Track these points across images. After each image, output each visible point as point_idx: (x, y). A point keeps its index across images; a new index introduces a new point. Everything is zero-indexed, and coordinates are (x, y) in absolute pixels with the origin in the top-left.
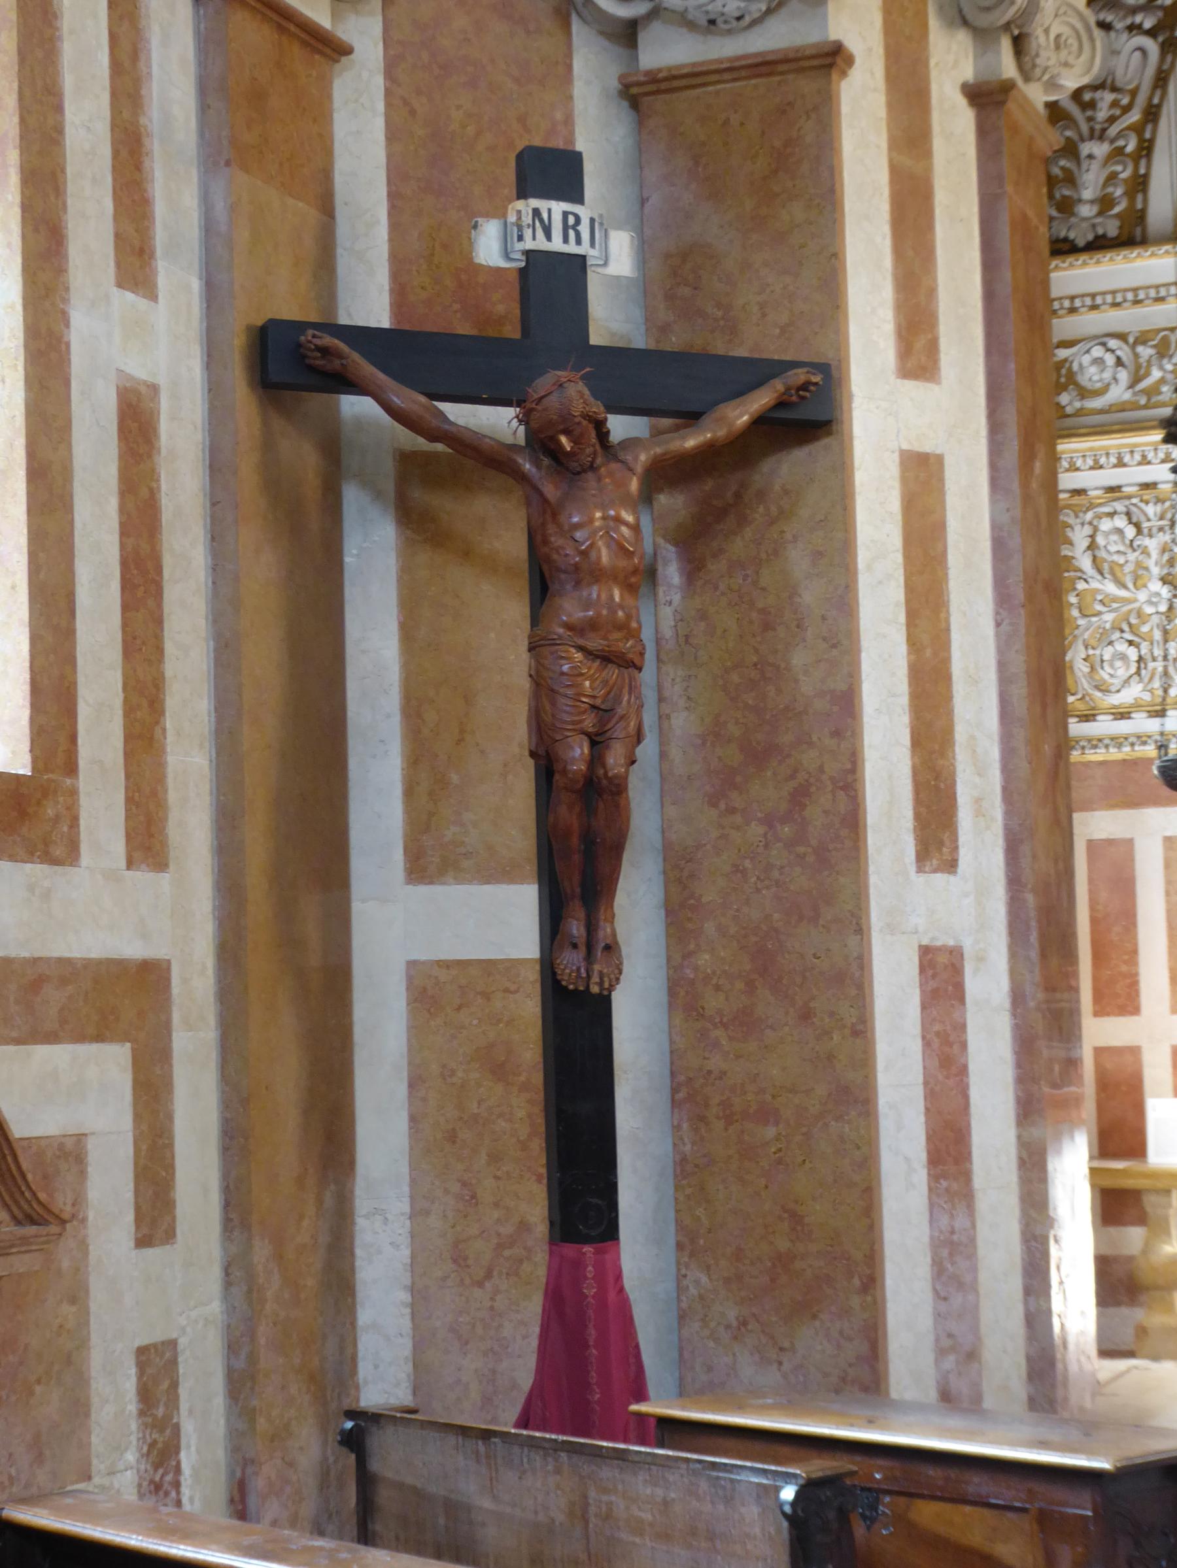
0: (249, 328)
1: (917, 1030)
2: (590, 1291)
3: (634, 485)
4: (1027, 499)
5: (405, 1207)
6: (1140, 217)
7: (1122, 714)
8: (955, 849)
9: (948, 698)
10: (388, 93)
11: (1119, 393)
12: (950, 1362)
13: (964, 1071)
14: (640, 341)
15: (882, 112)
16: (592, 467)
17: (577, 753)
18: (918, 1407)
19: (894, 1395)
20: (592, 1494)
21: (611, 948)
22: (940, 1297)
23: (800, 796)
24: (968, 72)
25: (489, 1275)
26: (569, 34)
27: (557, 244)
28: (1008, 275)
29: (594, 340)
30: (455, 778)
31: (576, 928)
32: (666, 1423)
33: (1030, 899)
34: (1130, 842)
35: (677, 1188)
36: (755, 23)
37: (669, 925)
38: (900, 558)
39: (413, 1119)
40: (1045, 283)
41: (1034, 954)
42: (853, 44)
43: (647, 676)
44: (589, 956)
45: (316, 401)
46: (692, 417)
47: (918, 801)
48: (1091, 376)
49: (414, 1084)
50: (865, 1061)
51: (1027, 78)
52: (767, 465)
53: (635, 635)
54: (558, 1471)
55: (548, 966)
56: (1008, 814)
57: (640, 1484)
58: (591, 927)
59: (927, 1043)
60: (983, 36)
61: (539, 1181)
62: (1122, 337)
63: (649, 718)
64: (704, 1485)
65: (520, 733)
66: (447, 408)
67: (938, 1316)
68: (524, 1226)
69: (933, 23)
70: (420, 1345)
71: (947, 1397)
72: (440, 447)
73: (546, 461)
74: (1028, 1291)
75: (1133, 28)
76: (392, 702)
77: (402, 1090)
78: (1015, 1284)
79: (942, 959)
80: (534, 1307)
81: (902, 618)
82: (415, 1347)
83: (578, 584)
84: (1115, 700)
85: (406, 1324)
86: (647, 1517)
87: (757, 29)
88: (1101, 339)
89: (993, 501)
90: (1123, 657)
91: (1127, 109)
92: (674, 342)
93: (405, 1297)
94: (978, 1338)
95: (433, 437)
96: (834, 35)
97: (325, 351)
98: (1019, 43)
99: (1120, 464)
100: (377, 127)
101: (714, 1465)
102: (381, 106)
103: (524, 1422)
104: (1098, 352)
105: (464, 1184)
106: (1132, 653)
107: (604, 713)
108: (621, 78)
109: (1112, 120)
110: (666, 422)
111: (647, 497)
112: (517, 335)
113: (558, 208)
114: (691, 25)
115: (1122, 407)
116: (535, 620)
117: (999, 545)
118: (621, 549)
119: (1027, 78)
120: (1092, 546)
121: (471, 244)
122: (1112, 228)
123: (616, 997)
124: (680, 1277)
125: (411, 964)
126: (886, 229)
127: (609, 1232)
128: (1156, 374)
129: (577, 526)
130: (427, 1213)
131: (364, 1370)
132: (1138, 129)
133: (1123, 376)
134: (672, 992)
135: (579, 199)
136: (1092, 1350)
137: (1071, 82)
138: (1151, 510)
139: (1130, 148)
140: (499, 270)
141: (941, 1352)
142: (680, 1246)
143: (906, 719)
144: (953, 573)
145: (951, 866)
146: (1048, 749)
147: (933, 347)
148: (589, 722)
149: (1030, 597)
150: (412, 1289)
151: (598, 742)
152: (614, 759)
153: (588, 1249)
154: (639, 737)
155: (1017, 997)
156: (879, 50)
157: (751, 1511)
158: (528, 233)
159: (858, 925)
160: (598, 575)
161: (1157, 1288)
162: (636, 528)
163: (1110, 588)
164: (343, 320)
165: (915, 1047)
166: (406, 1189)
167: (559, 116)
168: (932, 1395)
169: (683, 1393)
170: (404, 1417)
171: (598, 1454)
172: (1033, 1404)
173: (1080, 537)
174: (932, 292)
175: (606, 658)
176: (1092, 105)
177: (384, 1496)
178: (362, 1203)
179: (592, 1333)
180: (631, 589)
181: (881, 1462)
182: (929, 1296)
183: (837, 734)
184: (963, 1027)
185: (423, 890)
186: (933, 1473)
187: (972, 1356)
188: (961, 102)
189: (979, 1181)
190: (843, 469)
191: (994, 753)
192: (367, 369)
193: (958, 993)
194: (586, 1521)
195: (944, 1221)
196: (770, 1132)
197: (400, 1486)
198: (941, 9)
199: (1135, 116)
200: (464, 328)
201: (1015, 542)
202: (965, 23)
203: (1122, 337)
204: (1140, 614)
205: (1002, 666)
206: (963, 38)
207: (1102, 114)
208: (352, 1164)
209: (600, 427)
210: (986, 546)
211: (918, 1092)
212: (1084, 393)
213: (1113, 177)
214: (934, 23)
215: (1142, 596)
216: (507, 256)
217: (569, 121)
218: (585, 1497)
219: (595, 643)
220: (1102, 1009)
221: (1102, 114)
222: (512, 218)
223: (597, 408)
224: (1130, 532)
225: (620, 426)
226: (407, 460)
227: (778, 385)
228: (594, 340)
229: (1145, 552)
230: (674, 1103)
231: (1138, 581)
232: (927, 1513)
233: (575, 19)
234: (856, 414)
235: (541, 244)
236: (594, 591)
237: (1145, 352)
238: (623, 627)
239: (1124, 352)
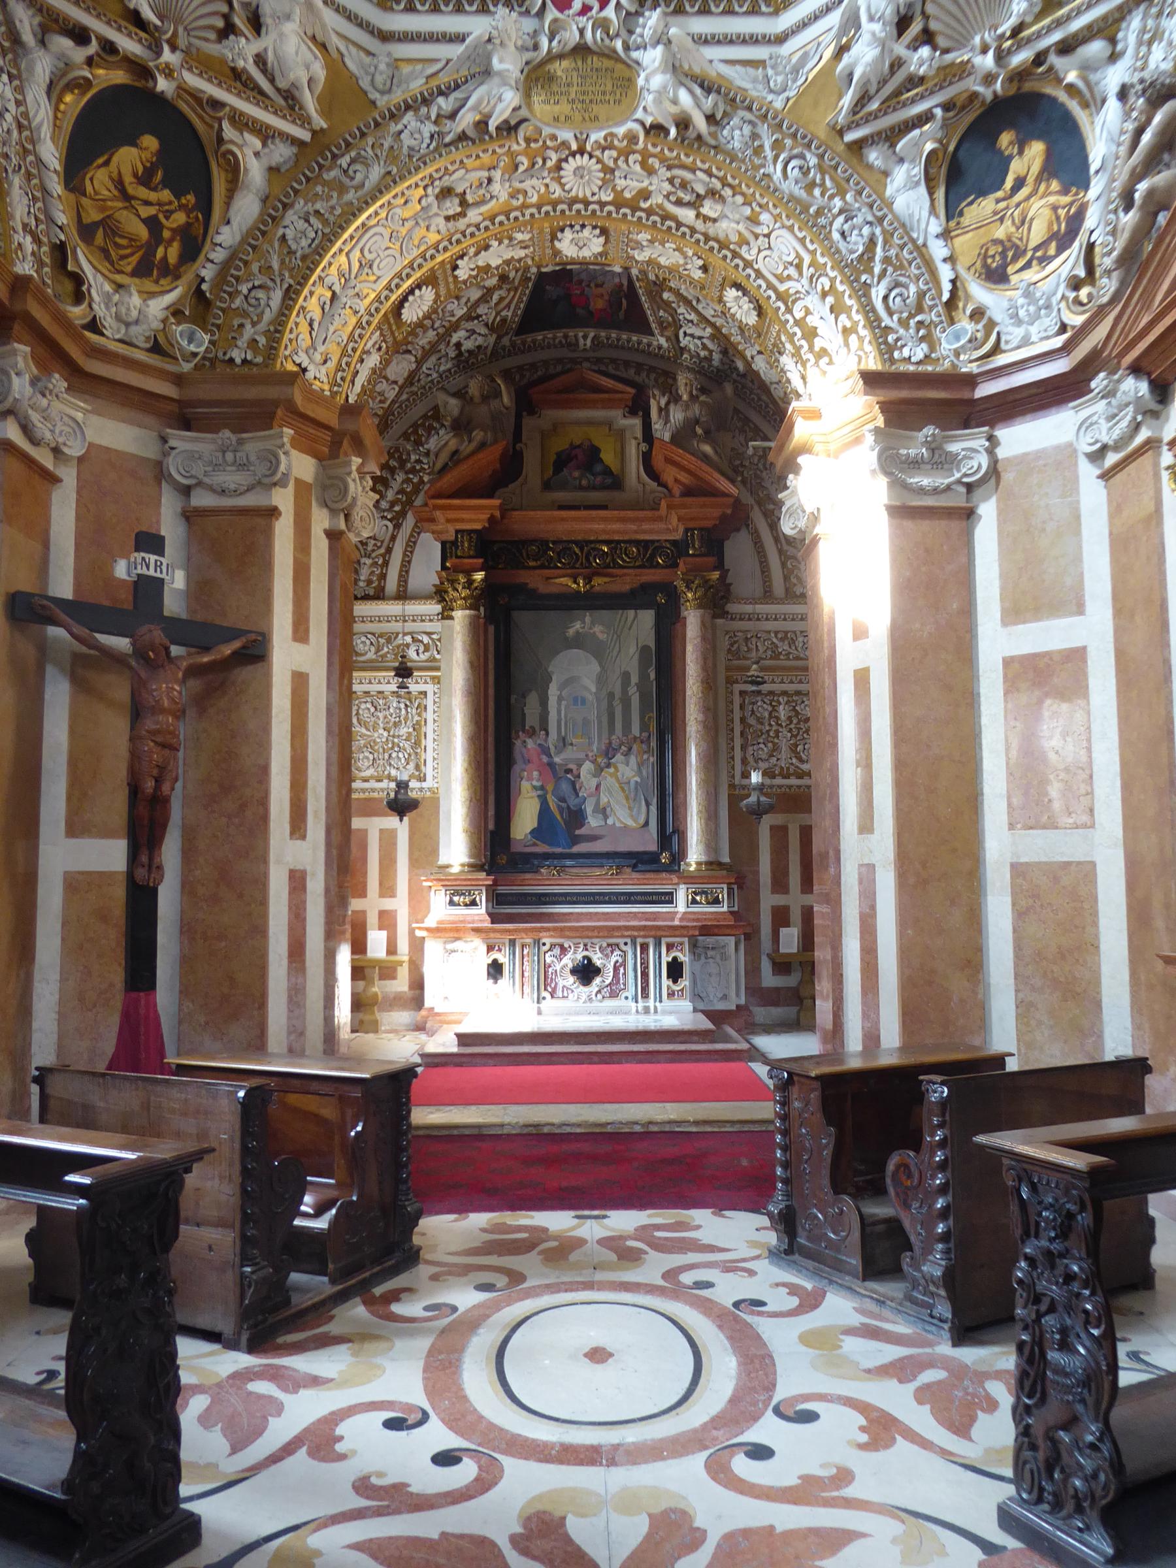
0: (7, 594)
1: (286, 903)
2: (142, 1011)
3: (180, 675)
4: (341, 693)
5: (58, 977)
6: (383, 589)
7: (366, 780)
8: (305, 830)
9: (306, 769)
10: (77, 500)
11: (371, 655)
12: (293, 1037)
13: (305, 919)
14: (184, 616)
15: (292, 536)
16: (162, 666)
17: (149, 785)
18: (279, 1056)
19: (270, 1050)
20: (152, 1098)
21: (160, 868)
22: (290, 1011)
23: (243, 807)
24: (326, 525)
25: (95, 1006)
26: (161, 488)
27: (151, 572)
28: (338, 604)
29: (166, 613)
30: (90, 793)
31: (144, 859)
32: (179, 1066)
33: (335, 852)
34: (366, 830)
35: (181, 967)
36: (241, 494)
37: (183, 858)
38: (289, 713)
39: (63, 939)
40: (352, 610)
41: (335, 874)
42: (281, 508)
43: (181, 754)
44: (150, 871)
45: (36, 627)
46: (206, 649)
47: (292, 811)
48: (360, 648)
49: (64, 924)
50: (264, 916)
51: (349, 530)
52: (236, 671)
53: (178, 737)
54: (137, 1089)
55: (130, 875)
56: (328, 817)
57: (175, 1093)
58: (151, 859)
59: (290, 908)
60: (333, 512)
61: (120, 964)
62: (373, 634)
63: (180, 771)
64: (204, 1092)
65: (123, 773)
66: (97, 635)
67: (289, 1018)
68: (112, 985)
69: (314, 503)
70: (61, 1038)
71: (291, 1050)
72: (92, 652)
73: (142, 662)
74: (325, 1007)
75: (383, 517)
76: (63, 759)
77: (59, 926)
78: (320, 1004)
79: (298, 875)
80: (115, 1020)
81: (289, 737)
82: (59, 1038)
83: (153, 714)
84: (363, 774)
85: (55, 1028)
86: (177, 1106)
87: (242, 497)
88: (365, 634)
89: (328, 693)
90: (367, 758)
91: (379, 548)
92: (199, 617)
93: (56, 1017)
94: (305, 1027)
95: (90, 647)
96: (274, 503)
97: (43, 607)
98: (347, 517)
99: (370, 683)
100: (72, 515)
101: (209, 1084)
102: (74, 506)
103: (109, 1068)
104: (363, 639)
105: (85, 967)
106: (371, 757)
107: (162, 769)
108: (183, 508)
109: (373, 551)
110: (193, 650)
111: (184, 681)
112: (131, 607)
113: (153, 558)
114: (214, 491)
115: (371, 661)
116: (132, 728)
117: (329, 711)
118: (172, 700)
119: (349, 530)
120: (357, 714)
121: (113, 568)
122: (372, 593)
123: (160, 888)
124: (180, 1005)
125: (65, 873)
126: (291, 582)
127: (151, 985)
128: (386, 650)
129: (156, 690)
130: (67, 980)
131: (34, 1048)
132: (383, 556)
133: (373, 649)
134: (183, 886)
135: (162, 554)
136: (348, 1029)
137: (366, 534)
138: (381, 702)
139: (380, 562)
140: (124, 580)
141: (289, 1033)
142: (181, 992)
143: (289, 777)
144: (310, 720)
145: (303, 837)
146: (344, 792)
147: (307, 631)
148: (155, 772)
149: (340, 733)
150: (59, 1013)
151: (158, 781)
152: (166, 788)
153: (142, 994)
154: (176, 780)
155: (327, 891)
156: (292, 511)
157: (224, 1102)
158: (139, 567)
159: (264, 859)
160: (163, 711)
161: (365, 1005)
162: (180, 693)
163: (364, 730)
164: (51, 594)
165: (286, 910)
166: (58, 969)
167: (154, 520)
168: (285, 1050)
169: (179, 1055)
170: (62, 1069)
171: (156, 1081)
172: (325, 1052)
173: (355, 708)
174: (308, 609)
175: (164, 746)
176: (366, 544)
177: (52, 1103)
178: (37, 976)
179: (142, 1029)
180: (177, 718)
181: (274, 1079)
182: (286, 1010)
183: (260, 782)
184: (305, 902)
185: (73, 841)
186: (296, 1082)
187: (302, 1034)
188: (324, 536)
189: (308, 963)
190: (268, 675)
191: (323, 793)
192: (63, 617)
193: (304, 888)
194: (149, 1110)
195: (300, 980)
196: (223, 944)
197: (61, 1099)
198: (317, 500)
199: (382, 551)
200: (107, 603)
201: (336, 710)
202: (327, 506)
203: (373, 634)
204: (374, 741)
205: (328, 759)
206: (325, 511)
207: (370, 548)
208: (33, 959)
209: (167, 649)
210: (324, 710)
211: (286, 928)
212: (358, 654)
213: (373, 572)
214: (314, 503)
215: (376, 735)
216: (129, 575)
217: (158, 522)
218: (149, 1099)
219: (159, 739)
220: (382, 895)
221: (370, 548)
222: (132, 560)
223: (166, 642)
224: (372, 710)
225: (175, 650)
226: (77, 658)
227: (244, 639)
228: (166, 613)
229: (378, 718)
230: (181, 932)
231: (375, 729)
232: (293, 1099)
233: (164, 483)
234: (275, 654)
235: (145, 571)
236: (161, 718)
237: (382, 641)
238: (170, 733)
239: (374, 640)
